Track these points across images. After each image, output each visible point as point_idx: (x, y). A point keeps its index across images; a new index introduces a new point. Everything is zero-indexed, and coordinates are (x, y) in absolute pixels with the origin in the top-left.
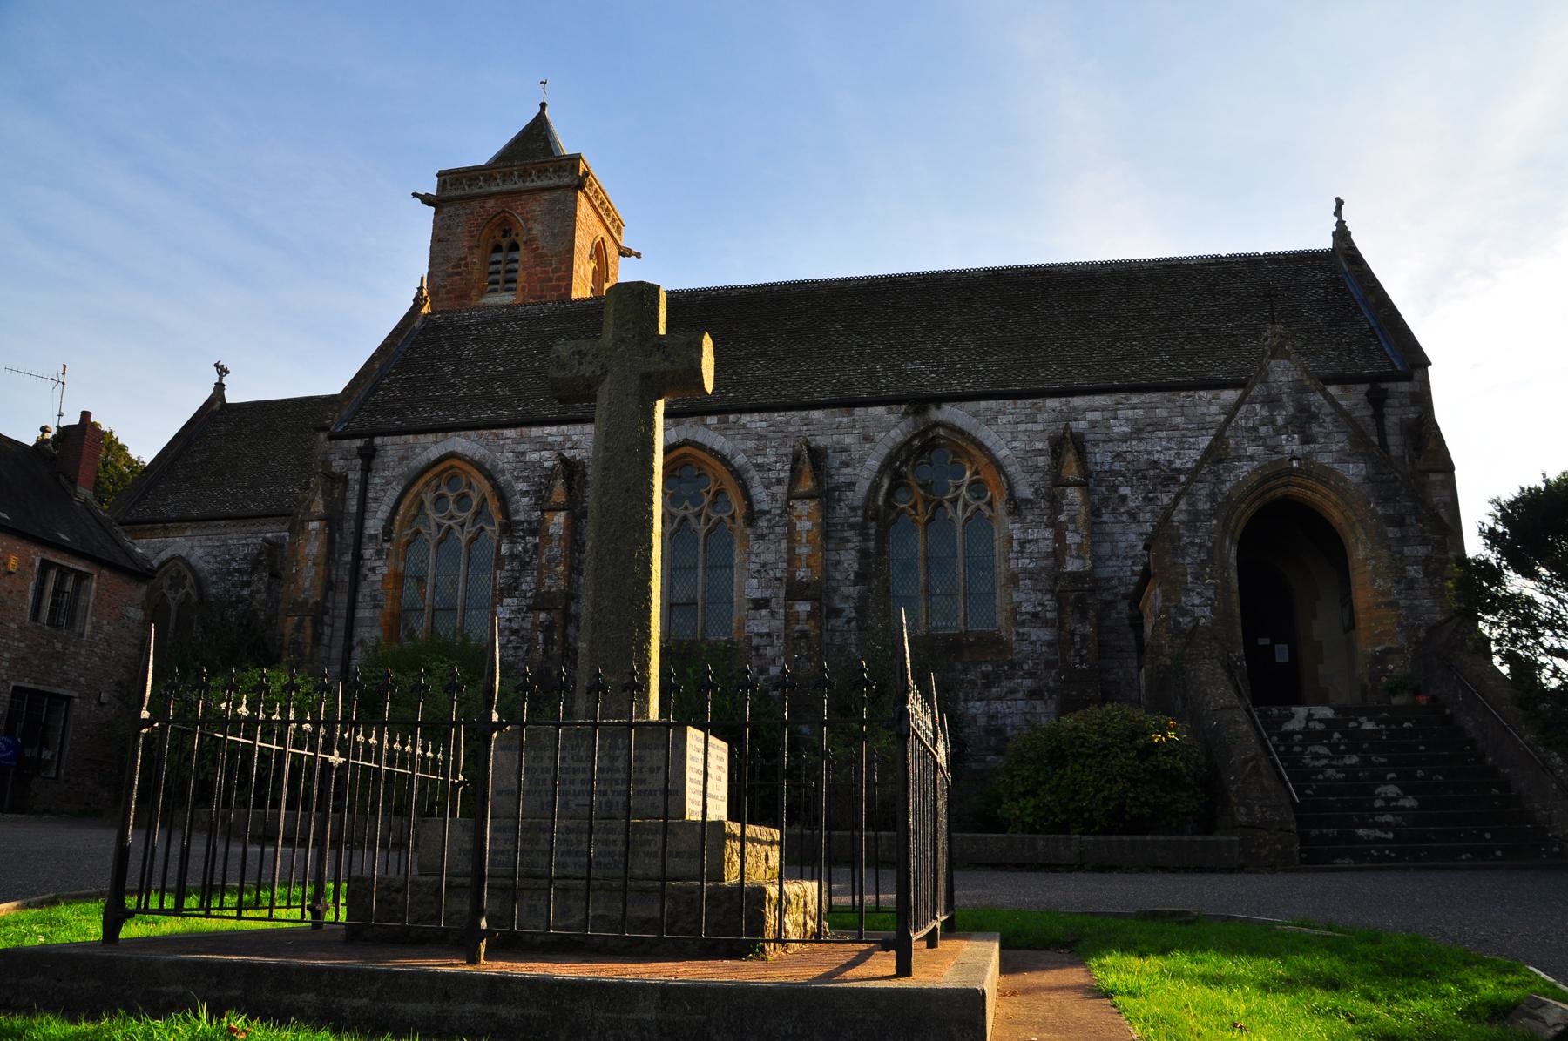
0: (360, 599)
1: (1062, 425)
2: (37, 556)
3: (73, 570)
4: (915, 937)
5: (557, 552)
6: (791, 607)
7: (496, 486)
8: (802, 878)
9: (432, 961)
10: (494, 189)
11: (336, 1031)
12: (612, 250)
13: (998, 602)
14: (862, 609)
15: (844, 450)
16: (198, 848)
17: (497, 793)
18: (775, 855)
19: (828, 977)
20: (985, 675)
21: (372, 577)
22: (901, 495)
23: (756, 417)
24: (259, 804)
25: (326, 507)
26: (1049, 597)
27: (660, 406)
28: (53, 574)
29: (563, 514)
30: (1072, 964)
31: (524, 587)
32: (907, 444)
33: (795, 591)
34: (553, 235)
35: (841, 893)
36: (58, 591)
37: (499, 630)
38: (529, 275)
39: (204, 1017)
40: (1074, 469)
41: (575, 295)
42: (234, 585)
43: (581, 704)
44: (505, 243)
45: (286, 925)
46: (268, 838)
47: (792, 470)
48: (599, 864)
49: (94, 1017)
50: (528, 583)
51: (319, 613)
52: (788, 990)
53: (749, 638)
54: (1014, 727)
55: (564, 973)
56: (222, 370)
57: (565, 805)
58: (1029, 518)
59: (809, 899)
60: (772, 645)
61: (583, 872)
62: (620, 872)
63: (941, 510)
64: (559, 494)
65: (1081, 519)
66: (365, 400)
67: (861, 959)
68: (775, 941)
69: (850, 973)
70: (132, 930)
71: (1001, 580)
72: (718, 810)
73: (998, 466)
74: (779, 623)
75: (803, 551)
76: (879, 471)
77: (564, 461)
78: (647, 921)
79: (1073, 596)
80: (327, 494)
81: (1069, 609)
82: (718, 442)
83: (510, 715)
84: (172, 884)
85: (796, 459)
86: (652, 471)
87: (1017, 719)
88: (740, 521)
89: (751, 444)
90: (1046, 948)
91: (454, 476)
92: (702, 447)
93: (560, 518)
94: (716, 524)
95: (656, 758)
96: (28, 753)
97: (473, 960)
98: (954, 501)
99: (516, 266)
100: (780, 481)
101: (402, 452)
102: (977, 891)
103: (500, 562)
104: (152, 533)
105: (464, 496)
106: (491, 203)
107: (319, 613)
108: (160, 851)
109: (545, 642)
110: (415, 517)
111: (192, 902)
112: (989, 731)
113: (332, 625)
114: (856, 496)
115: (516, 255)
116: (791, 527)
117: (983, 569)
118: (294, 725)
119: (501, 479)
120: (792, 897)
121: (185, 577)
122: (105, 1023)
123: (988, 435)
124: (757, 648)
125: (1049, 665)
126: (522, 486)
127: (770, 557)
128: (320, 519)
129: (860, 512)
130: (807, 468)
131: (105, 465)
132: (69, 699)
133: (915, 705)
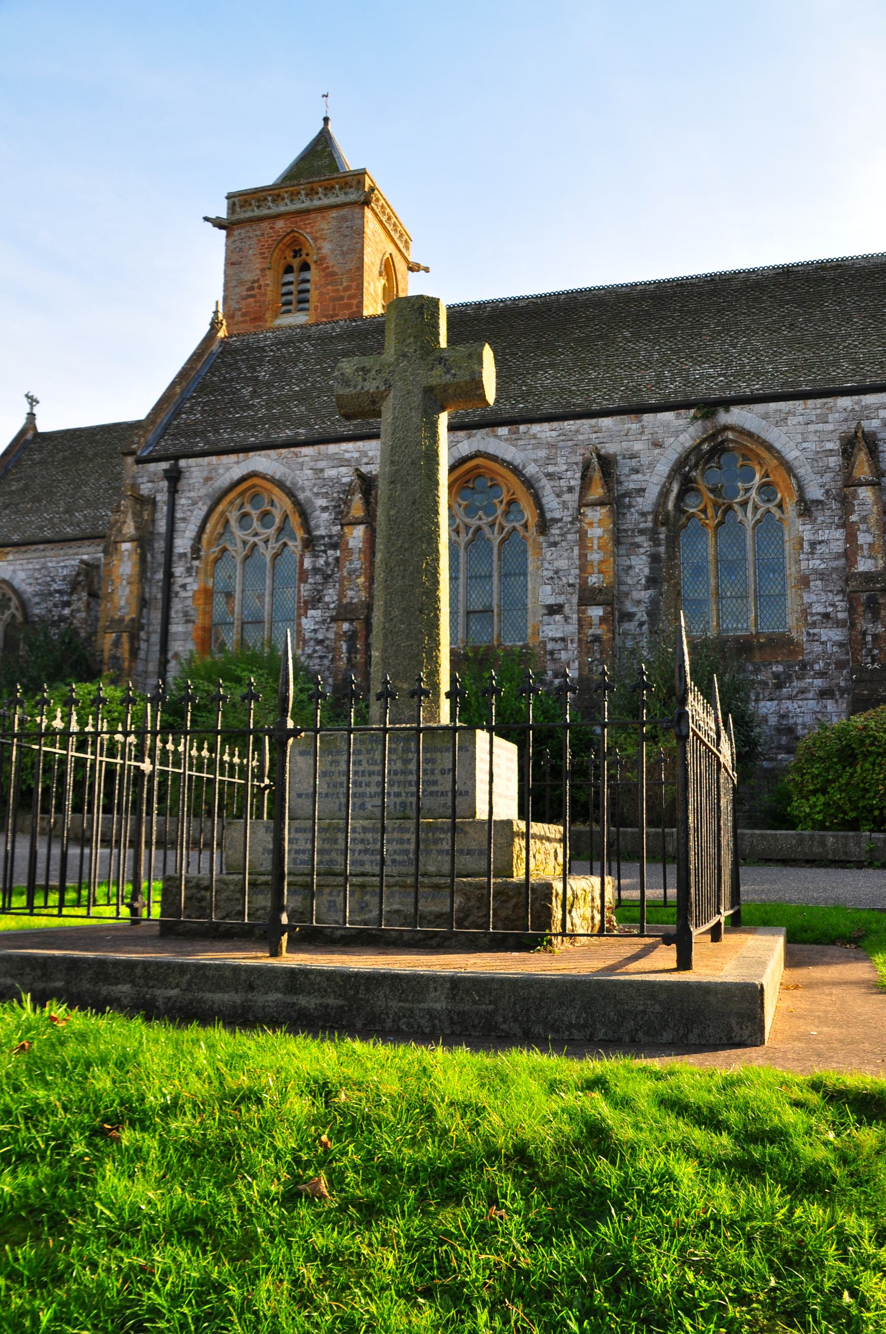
0: (173, 614)
1: (854, 425)
4: (695, 932)
5: (357, 564)
7: (297, 503)
8: (592, 874)
10: (283, 209)
11: (148, 1019)
13: (789, 603)
14: (653, 614)
15: (633, 456)
16: (22, 849)
19: (611, 969)
20: (776, 676)
21: (183, 594)
22: (690, 499)
23: (546, 426)
25: (137, 529)
26: (840, 597)
27: (443, 419)
30: (857, 959)
31: (327, 599)
32: (697, 448)
33: (588, 597)
34: (343, 254)
35: (629, 887)
38: (321, 294)
39: (28, 1005)
40: (866, 469)
41: (366, 313)
42: (55, 606)
43: (375, 709)
44: (296, 263)
46: (84, 841)
47: (583, 477)
48: (394, 861)
50: (330, 595)
51: (135, 629)
52: (571, 982)
53: (544, 643)
54: (804, 726)
55: (360, 965)
56: (32, 401)
58: (820, 519)
60: (566, 649)
61: (377, 870)
62: (412, 869)
63: (730, 513)
64: (357, 509)
65: (872, 520)
66: (169, 424)
71: (791, 581)
72: (507, 807)
73: (788, 468)
74: (572, 628)
75: (594, 557)
76: (669, 477)
77: (361, 476)
78: (439, 916)
79: (864, 597)
80: (137, 515)
81: (860, 609)
82: (508, 452)
83: (307, 724)
84: (55, 882)
85: (586, 467)
86: (437, 483)
87: (808, 719)
88: (532, 529)
90: (833, 943)
91: (256, 495)
92: (494, 458)
93: (359, 532)
94: (509, 533)
97: (275, 953)
98: (744, 504)
100: (570, 489)
102: (763, 885)
105: (266, 514)
106: (280, 224)
107: (135, 629)
109: (349, 651)
110: (222, 535)
112: (780, 730)
113: (147, 641)
114: (647, 502)
115: (306, 275)
116: (583, 534)
117: (774, 571)
118: (106, 736)
119: (301, 496)
120: (579, 892)
121: (10, 599)
123: (776, 436)
124: (552, 653)
125: (841, 665)
126: (321, 502)
127: (562, 564)
128: (131, 540)
129: (650, 518)
130: (597, 475)
133: (695, 705)
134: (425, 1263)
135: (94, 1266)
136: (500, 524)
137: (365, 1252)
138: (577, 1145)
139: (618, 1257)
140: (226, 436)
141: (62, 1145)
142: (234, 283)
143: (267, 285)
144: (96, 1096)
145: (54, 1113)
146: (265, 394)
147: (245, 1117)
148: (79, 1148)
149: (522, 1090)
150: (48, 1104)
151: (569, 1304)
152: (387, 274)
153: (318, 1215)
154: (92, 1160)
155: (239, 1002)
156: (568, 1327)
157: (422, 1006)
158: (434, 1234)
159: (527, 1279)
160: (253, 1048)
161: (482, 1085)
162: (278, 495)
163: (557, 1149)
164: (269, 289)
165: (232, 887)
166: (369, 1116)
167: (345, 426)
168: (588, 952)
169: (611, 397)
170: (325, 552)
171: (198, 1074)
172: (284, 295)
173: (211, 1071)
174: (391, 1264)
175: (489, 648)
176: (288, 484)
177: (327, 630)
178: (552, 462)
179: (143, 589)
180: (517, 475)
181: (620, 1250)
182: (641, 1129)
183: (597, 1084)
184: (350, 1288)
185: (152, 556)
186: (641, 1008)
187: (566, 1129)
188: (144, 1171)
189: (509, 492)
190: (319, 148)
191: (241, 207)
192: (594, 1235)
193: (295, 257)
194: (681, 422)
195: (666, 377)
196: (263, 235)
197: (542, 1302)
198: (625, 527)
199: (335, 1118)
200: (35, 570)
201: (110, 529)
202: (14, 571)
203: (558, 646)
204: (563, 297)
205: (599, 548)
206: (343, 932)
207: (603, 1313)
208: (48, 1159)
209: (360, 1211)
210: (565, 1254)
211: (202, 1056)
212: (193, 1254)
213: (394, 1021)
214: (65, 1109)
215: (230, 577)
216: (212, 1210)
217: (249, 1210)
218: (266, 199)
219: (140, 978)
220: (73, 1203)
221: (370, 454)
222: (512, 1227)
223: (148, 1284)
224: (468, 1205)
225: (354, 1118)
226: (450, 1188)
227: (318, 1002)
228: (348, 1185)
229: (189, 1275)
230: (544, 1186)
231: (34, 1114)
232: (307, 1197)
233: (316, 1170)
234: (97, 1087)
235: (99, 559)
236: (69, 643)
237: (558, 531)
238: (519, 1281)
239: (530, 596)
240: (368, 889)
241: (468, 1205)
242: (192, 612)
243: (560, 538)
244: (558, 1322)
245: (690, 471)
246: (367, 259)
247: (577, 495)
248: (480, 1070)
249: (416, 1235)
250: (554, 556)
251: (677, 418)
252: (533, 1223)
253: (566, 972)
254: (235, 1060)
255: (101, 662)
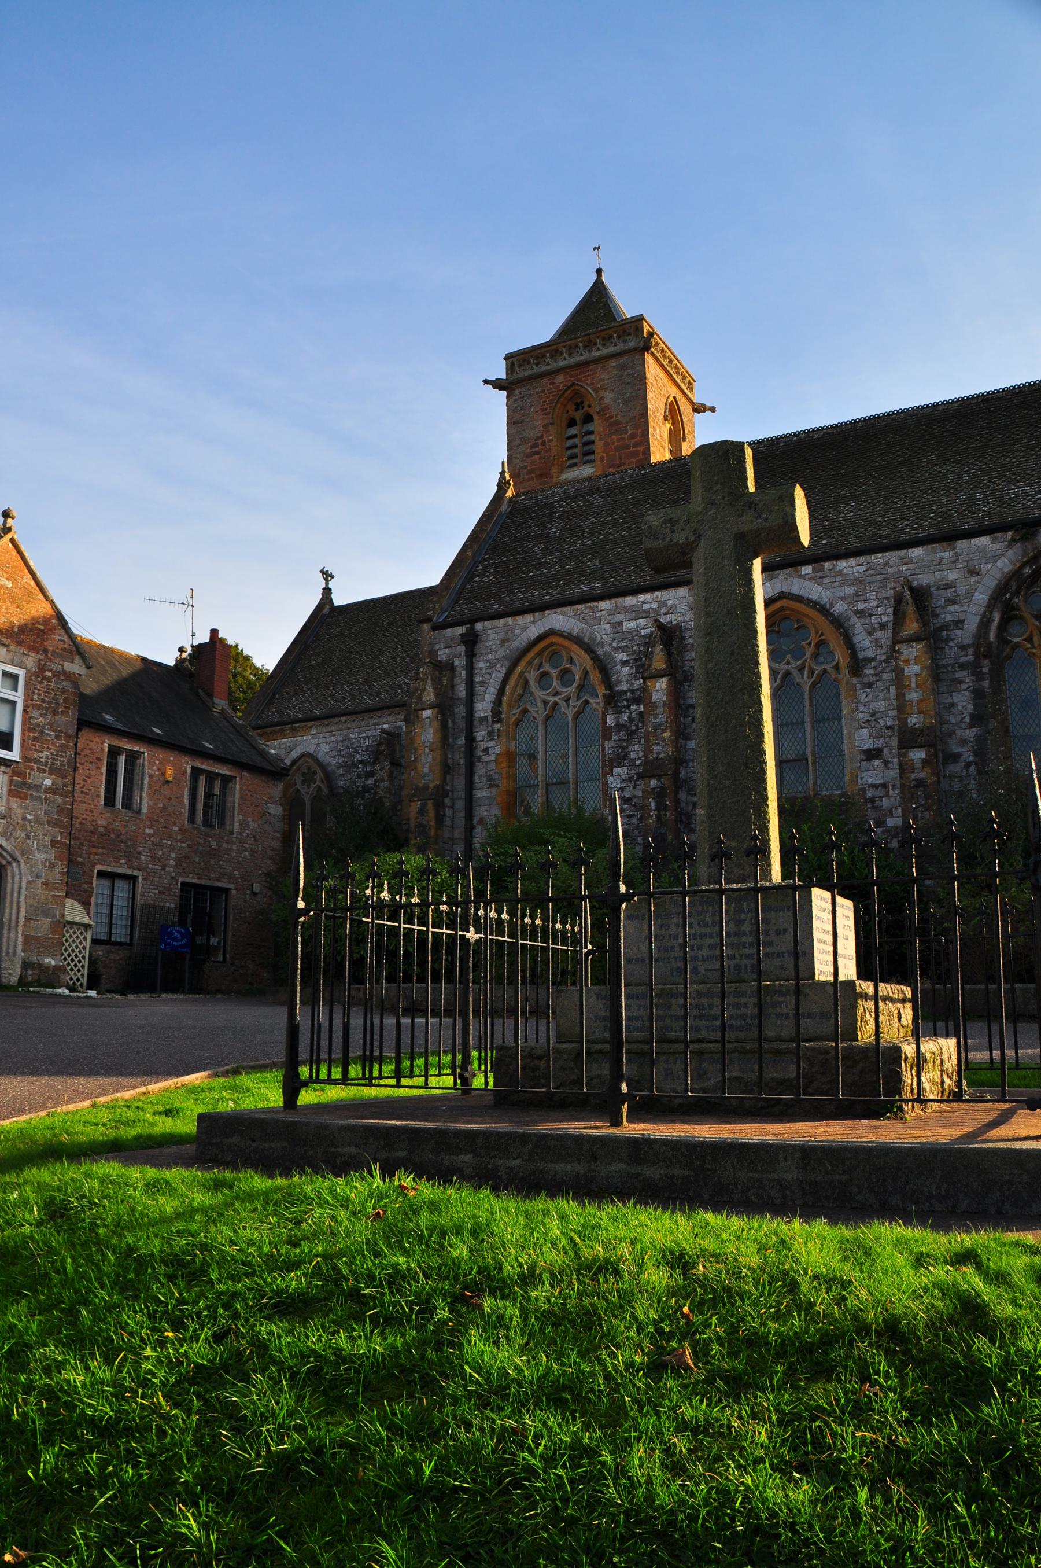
0: (476, 779)
2: (188, 764)
3: (218, 775)
5: (662, 718)
6: (905, 755)
7: (596, 659)
8: (935, 1035)
9: (577, 1124)
10: (562, 363)
11: (495, 1189)
12: (685, 408)
14: (980, 751)
15: (948, 586)
16: (357, 1021)
17: (628, 961)
18: (908, 1013)
19: (971, 1137)
22: (1014, 628)
23: (852, 561)
24: (408, 979)
25: (436, 695)
27: (757, 564)
28: (202, 780)
29: (665, 680)
31: (632, 756)
32: (1016, 574)
33: (908, 739)
34: (626, 402)
35: (978, 1049)
36: (208, 795)
37: (617, 798)
38: (606, 444)
39: (377, 1174)
41: (654, 459)
42: (359, 776)
44: (578, 416)
45: (437, 1091)
47: (895, 613)
48: (731, 1026)
49: (287, 1173)
50: (636, 752)
53: (864, 790)
55: (704, 1134)
56: (327, 576)
57: (694, 971)
59: (945, 1057)
60: (887, 795)
61: (718, 1035)
64: (659, 661)
67: (1003, 1118)
68: (913, 1101)
69: (995, 1133)
70: (306, 1097)
72: (848, 970)
74: (893, 773)
75: (913, 696)
77: (661, 627)
78: (782, 1082)
80: (437, 682)
82: (815, 592)
84: (337, 1054)
85: (898, 601)
86: (755, 632)
88: (845, 671)
89: (850, 590)
91: (554, 654)
92: (799, 599)
94: (820, 676)
95: (783, 919)
96: (199, 940)
97: (616, 1123)
99: (592, 437)
100: (883, 626)
101: (502, 635)
103: (607, 733)
104: (282, 734)
105: (566, 672)
106: (560, 379)
107: (440, 796)
108: (325, 1024)
109: (658, 808)
110: (521, 696)
111: (354, 1071)
113: (452, 807)
114: (966, 634)
115: (591, 427)
116: (899, 672)
119: (601, 652)
120: (928, 1055)
121: (315, 773)
122: (296, 1179)
124: (872, 800)
126: (621, 656)
127: (879, 705)
129: (971, 651)
130: (910, 609)
131: (235, 676)
132: (227, 891)
134: (798, 1438)
135: (468, 1426)
136: (810, 667)
137: (736, 1425)
138: (951, 1321)
139: (1004, 1440)
140: (520, 596)
141: (427, 1310)
142: (518, 442)
143: (551, 440)
144: (453, 1263)
145: (415, 1279)
146: (557, 551)
147: (603, 1287)
148: (443, 1314)
149: (888, 1263)
150: (409, 1269)
151: (953, 1486)
152: (672, 418)
153: (685, 1387)
154: (455, 1325)
155: (582, 1172)
156: (954, 1509)
157: (772, 1176)
158: (806, 1410)
159: (907, 1458)
160: (605, 1218)
161: (846, 1258)
162: (577, 651)
163: (930, 1325)
164: (554, 444)
165: (565, 1056)
166: (730, 1289)
167: (641, 577)
168: (942, 1120)
169: (920, 526)
170: (628, 707)
171: (553, 1244)
172: (568, 448)
173: (564, 1242)
174: (763, 1438)
175: (806, 798)
176: (586, 639)
177: (634, 788)
178: (862, 598)
179: (446, 755)
180: (825, 615)
181: (1007, 1433)
182: (1021, 1306)
183: (965, 1257)
184: (723, 1460)
185: (453, 721)
186: (1007, 1178)
187: (939, 1304)
188: (507, 1337)
189: (817, 633)
190: (594, 300)
191: (520, 366)
192: (976, 1416)
193: (577, 410)
194: (998, 546)
195: (979, 500)
196: (543, 391)
197: (924, 1483)
198: (944, 662)
199: (695, 1290)
200: (338, 742)
201: (411, 697)
202: (318, 745)
203: (880, 792)
204: (860, 424)
205: (917, 687)
206: (681, 1101)
207: (992, 1498)
208: (414, 1323)
209: (727, 1383)
210: (942, 1436)
211: (554, 1227)
212: (563, 1420)
213: (742, 1192)
214: (427, 1277)
215: (532, 739)
216: (578, 1377)
217: (615, 1379)
218: (544, 356)
219: (481, 1148)
220: (442, 1365)
221: (669, 603)
222: (887, 1404)
223: (522, 1446)
224: (839, 1381)
225: (714, 1291)
226: (818, 1363)
227: (663, 1172)
228: (713, 1357)
229: (560, 1440)
230: (918, 1363)
231: (397, 1278)
232: (672, 1368)
233: (679, 1342)
234: (455, 1255)
235: (400, 727)
236: (375, 813)
237: (872, 672)
238: (898, 1460)
239: (845, 741)
240: (706, 1056)
241: (839, 1381)
242: (496, 776)
243: (875, 679)
244: (943, 1505)
245: (1011, 598)
246: (650, 405)
247: (890, 631)
248: (841, 1242)
249: (787, 1409)
250: (870, 696)
251: (993, 542)
252: (909, 1401)
253: (924, 1140)
254: (589, 1230)
255: (408, 830)
